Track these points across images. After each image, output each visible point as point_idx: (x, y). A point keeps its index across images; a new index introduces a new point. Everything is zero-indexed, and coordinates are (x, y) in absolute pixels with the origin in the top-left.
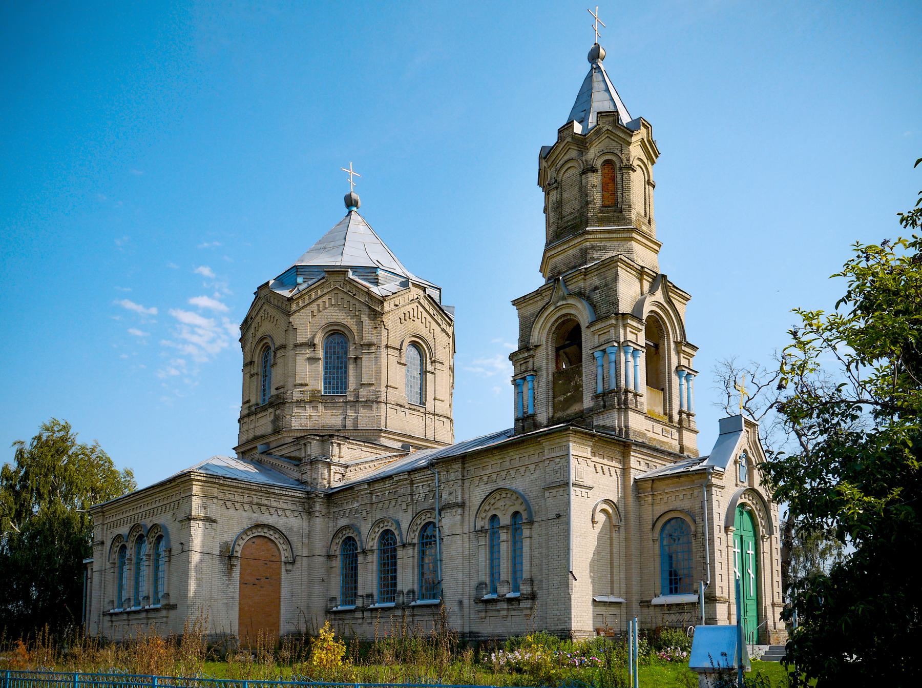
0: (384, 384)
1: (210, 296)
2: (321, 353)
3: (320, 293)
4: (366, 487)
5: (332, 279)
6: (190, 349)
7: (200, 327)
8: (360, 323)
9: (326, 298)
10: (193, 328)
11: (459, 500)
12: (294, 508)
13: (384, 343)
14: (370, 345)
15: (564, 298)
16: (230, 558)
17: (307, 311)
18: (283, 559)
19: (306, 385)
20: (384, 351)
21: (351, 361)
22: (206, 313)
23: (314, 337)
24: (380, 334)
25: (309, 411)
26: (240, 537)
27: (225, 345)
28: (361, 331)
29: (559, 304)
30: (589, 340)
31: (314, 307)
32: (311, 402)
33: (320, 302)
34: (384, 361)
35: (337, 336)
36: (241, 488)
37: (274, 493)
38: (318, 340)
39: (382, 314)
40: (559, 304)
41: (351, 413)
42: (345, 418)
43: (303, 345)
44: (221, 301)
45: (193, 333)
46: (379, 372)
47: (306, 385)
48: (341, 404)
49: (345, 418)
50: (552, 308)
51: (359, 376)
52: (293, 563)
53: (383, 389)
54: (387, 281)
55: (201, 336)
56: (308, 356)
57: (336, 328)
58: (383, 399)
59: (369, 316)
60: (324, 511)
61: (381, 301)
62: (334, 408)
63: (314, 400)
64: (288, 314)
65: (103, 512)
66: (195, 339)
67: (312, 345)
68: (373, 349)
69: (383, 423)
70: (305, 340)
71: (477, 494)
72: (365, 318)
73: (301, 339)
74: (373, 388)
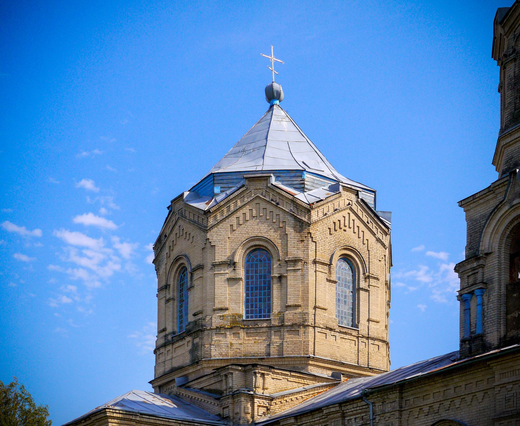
0: (311, 304)
1: (96, 213)
2: (241, 273)
3: (239, 204)
4: (293, 421)
5: (253, 186)
6: (81, 274)
7: (87, 248)
8: (284, 236)
9: (246, 210)
10: (80, 250)
13: (311, 258)
14: (296, 261)
17: (226, 225)
19: (227, 309)
20: (311, 268)
21: (275, 281)
22: (93, 232)
23: (234, 254)
24: (307, 248)
25: (230, 338)
27: (117, 267)
28: (285, 245)
29: (515, 202)
31: (233, 220)
32: (231, 328)
33: (240, 214)
34: (311, 278)
35: (259, 253)
38: (239, 258)
39: (309, 225)
40: (515, 202)
41: (275, 339)
42: (269, 345)
43: (222, 264)
44: (108, 217)
45: (81, 255)
46: (306, 291)
47: (227, 309)
48: (264, 330)
49: (269, 345)
50: (506, 208)
51: (284, 297)
53: (311, 311)
54: (315, 185)
55: (90, 258)
56: (227, 276)
57: (257, 243)
58: (311, 322)
59: (294, 228)
61: (308, 209)
62: (258, 334)
63: (235, 325)
64: (205, 230)
66: (84, 262)
67: (231, 264)
68: (299, 266)
69: (311, 349)
70: (224, 259)
72: (290, 230)
73: (221, 256)
74: (299, 310)
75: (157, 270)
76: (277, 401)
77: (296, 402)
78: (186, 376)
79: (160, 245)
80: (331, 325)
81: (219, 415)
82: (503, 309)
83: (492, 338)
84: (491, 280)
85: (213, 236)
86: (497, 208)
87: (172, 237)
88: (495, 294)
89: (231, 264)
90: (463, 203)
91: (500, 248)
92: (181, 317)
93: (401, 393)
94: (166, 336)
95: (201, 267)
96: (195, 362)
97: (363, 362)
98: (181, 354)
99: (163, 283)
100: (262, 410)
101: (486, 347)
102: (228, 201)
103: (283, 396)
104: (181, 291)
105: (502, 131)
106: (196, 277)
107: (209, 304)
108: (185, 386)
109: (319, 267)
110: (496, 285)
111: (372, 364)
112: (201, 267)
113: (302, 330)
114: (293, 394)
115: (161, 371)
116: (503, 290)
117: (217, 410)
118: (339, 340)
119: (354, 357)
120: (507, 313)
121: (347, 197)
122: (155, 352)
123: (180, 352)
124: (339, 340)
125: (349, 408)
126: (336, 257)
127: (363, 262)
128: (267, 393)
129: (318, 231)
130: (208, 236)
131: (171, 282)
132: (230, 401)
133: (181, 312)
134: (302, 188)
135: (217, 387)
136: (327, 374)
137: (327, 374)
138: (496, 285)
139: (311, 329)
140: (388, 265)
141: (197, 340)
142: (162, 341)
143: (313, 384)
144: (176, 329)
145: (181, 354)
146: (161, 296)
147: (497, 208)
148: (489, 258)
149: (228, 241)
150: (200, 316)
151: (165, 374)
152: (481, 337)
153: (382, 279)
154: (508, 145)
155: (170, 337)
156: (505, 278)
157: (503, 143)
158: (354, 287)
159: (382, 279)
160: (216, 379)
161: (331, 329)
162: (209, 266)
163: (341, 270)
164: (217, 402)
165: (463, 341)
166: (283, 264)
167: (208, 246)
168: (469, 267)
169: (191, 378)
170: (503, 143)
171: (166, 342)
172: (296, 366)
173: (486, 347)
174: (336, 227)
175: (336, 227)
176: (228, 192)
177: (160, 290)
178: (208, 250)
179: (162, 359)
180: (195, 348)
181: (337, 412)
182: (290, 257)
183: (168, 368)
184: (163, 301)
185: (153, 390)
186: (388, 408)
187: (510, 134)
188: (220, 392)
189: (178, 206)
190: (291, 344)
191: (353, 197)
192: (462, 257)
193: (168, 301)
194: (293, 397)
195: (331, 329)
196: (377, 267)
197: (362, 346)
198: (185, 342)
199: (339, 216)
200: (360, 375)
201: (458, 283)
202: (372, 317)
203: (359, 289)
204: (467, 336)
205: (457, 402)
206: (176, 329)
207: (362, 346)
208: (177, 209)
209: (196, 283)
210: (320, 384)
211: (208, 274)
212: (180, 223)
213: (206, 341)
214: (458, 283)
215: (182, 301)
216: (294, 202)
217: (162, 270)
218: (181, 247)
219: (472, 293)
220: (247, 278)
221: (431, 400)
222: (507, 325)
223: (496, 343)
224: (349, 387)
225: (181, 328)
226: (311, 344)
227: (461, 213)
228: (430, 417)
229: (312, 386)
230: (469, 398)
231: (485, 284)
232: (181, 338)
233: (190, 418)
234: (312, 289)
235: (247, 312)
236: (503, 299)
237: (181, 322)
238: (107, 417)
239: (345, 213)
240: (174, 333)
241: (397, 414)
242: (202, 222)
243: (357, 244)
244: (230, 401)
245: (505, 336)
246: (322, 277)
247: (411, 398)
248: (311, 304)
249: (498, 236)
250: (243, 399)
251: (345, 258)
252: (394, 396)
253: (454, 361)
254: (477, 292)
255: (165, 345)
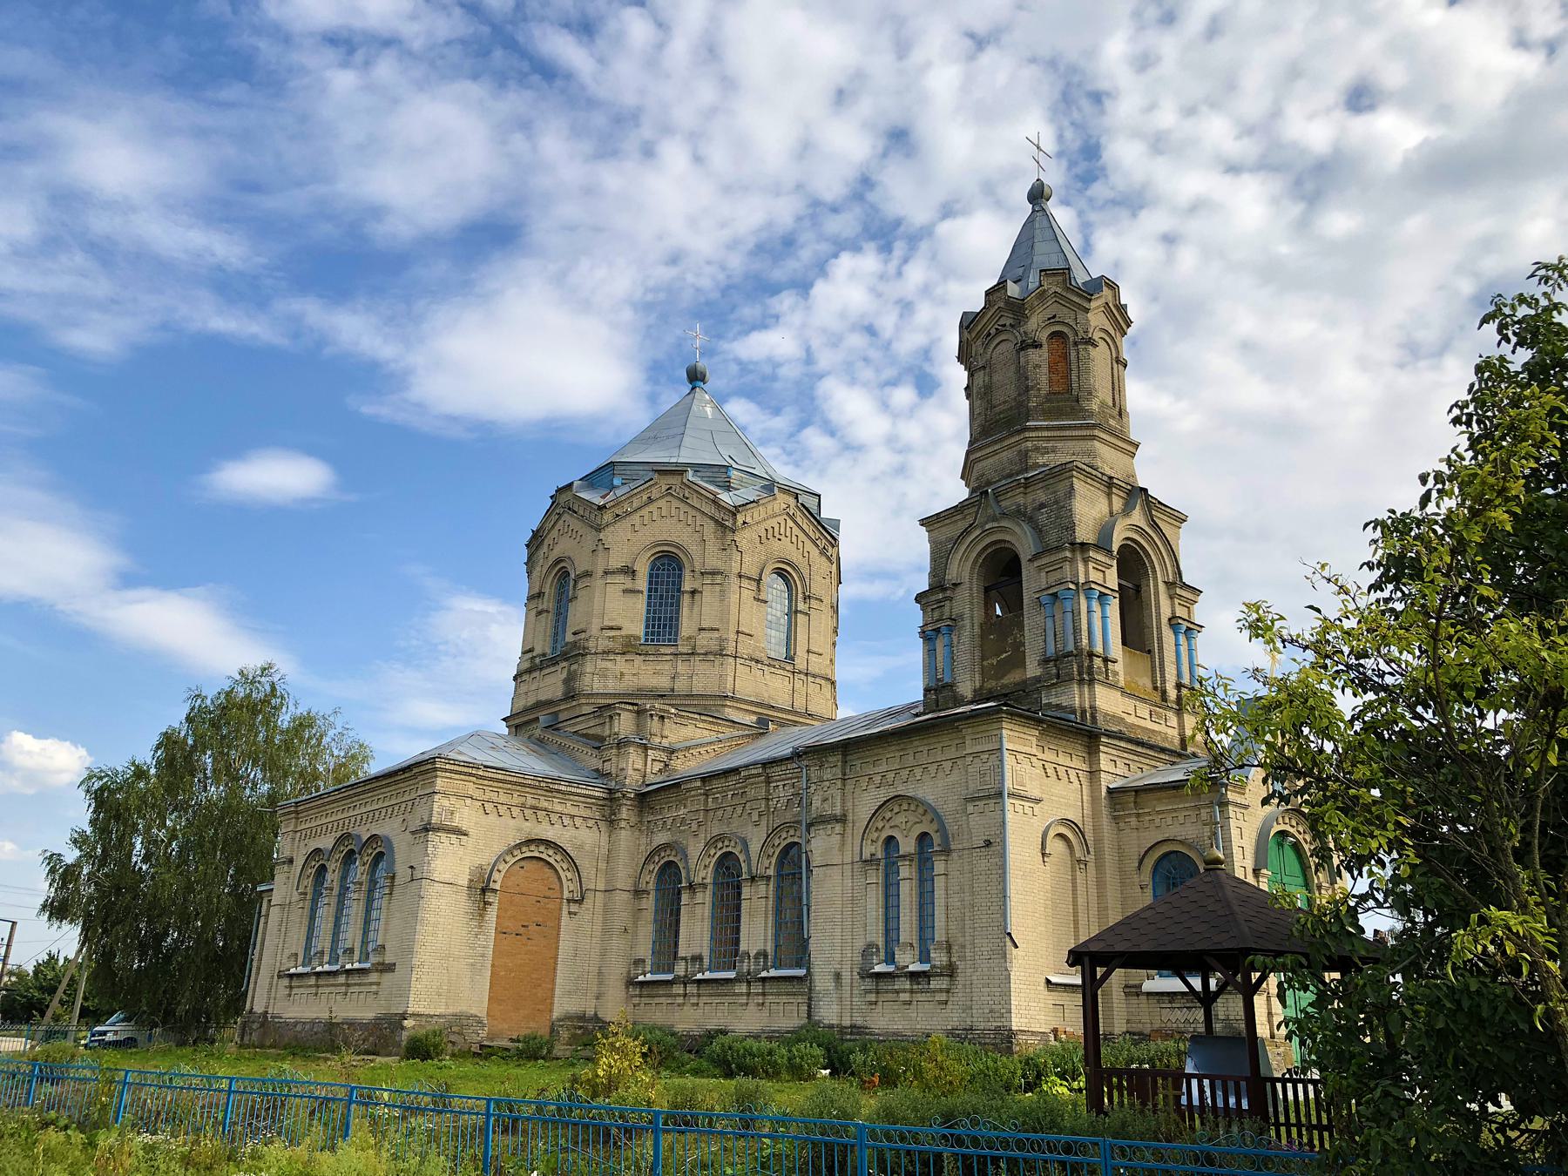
2: (642, 583)
4: (699, 784)
11: (838, 811)
12: (587, 813)
13: (736, 570)
15: (994, 519)
16: (484, 891)
18: (566, 895)
26: (501, 858)
30: (1033, 581)
34: (734, 598)
35: (668, 567)
36: (510, 783)
37: (559, 791)
38: (643, 569)
52: (580, 902)
53: (733, 636)
58: (730, 650)
60: (633, 820)
63: (629, 648)
65: (297, 812)
71: (865, 803)
73: (616, 562)
75: (529, 573)
76: (680, 755)
77: (706, 757)
78: (556, 714)
79: (536, 541)
80: (758, 655)
81: (597, 770)
82: (978, 654)
83: (966, 688)
84: (961, 617)
85: (607, 536)
86: (966, 532)
87: (554, 533)
88: (966, 635)
89: (629, 571)
90: (924, 522)
91: (971, 579)
92: (556, 634)
93: (845, 755)
94: (533, 658)
95: (588, 574)
96: (571, 695)
97: (799, 705)
98: (551, 685)
99: (536, 590)
100: (658, 766)
101: (959, 701)
102: (630, 497)
103: (688, 748)
104: (559, 601)
105: (971, 443)
106: (580, 585)
107: (595, 621)
108: (553, 727)
109: (745, 583)
110: (967, 622)
111: (812, 709)
112: (588, 574)
113: (719, 660)
114: (701, 745)
115: (521, 704)
116: (977, 630)
117: (595, 763)
118: (768, 677)
119: (787, 698)
120: (983, 658)
121: (782, 500)
122: (515, 678)
123: (550, 680)
124: (768, 677)
125: (776, 771)
126: (767, 571)
127: (802, 579)
128: (665, 743)
129: (744, 538)
130: (601, 536)
131: (547, 590)
132: (614, 751)
133: (556, 627)
134: (728, 488)
135: (597, 731)
136: (750, 719)
137: (750, 719)
138: (967, 622)
139: (731, 660)
140: (834, 583)
141: (574, 667)
142: (527, 665)
143: (729, 732)
144: (548, 651)
145: (551, 685)
146: (532, 606)
147: (966, 532)
148: (959, 590)
149: (629, 542)
150: (583, 636)
151: (526, 710)
152: (950, 686)
153: (827, 600)
154: (979, 460)
155: (537, 660)
156: (979, 615)
157: (972, 457)
158: (790, 607)
159: (827, 600)
160: (597, 721)
161: (757, 661)
162: (600, 573)
163: (775, 588)
164: (595, 752)
165: (927, 690)
166: (697, 575)
167: (600, 547)
168: (933, 598)
169: (562, 717)
170: (972, 457)
171: (532, 666)
172: (707, 706)
173: (959, 701)
174: (770, 534)
175: (770, 534)
176: (632, 485)
177: (531, 598)
178: (601, 553)
179: (524, 688)
180: (570, 679)
181: (759, 775)
182: (708, 568)
183: (531, 701)
184: (534, 613)
185: (506, 731)
186: (827, 774)
187: (980, 449)
188: (602, 739)
189: (563, 498)
190: (703, 678)
191: (792, 501)
192: (924, 586)
193: (539, 613)
194: (702, 750)
195: (757, 661)
196: (818, 587)
197: (798, 684)
198: (558, 668)
199: (773, 522)
200: (795, 723)
201: (920, 569)
202: (813, 648)
203: (796, 612)
204: (933, 684)
205: (918, 771)
206: (548, 651)
207: (798, 684)
208: (563, 502)
209: (580, 593)
210: (736, 733)
211: (598, 583)
212: (566, 517)
213: (589, 668)
214: (920, 569)
215: (558, 614)
216: (716, 502)
217: (536, 574)
218: (563, 546)
219: (937, 631)
220: (650, 590)
221: (883, 768)
222: (983, 673)
223: (969, 695)
224: (779, 743)
225: (554, 649)
226: (730, 679)
227: (922, 536)
228: (883, 791)
229: (728, 735)
230: (933, 768)
231: (954, 623)
232: (554, 662)
233: (555, 774)
234: (734, 610)
235: (647, 634)
236: (977, 640)
237: (556, 641)
238: (435, 769)
239: (781, 519)
240: (544, 655)
241: (839, 783)
242: (595, 518)
243: (795, 557)
244: (614, 751)
245: (981, 687)
246: (748, 595)
247: (858, 763)
248: (733, 628)
249: (969, 564)
250: (631, 750)
251: (780, 573)
252: (836, 759)
253: (917, 715)
254: (944, 630)
255: (529, 671)
